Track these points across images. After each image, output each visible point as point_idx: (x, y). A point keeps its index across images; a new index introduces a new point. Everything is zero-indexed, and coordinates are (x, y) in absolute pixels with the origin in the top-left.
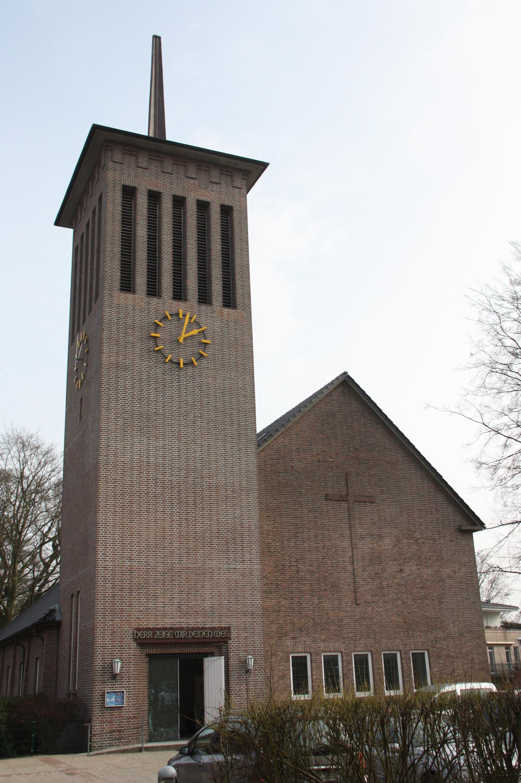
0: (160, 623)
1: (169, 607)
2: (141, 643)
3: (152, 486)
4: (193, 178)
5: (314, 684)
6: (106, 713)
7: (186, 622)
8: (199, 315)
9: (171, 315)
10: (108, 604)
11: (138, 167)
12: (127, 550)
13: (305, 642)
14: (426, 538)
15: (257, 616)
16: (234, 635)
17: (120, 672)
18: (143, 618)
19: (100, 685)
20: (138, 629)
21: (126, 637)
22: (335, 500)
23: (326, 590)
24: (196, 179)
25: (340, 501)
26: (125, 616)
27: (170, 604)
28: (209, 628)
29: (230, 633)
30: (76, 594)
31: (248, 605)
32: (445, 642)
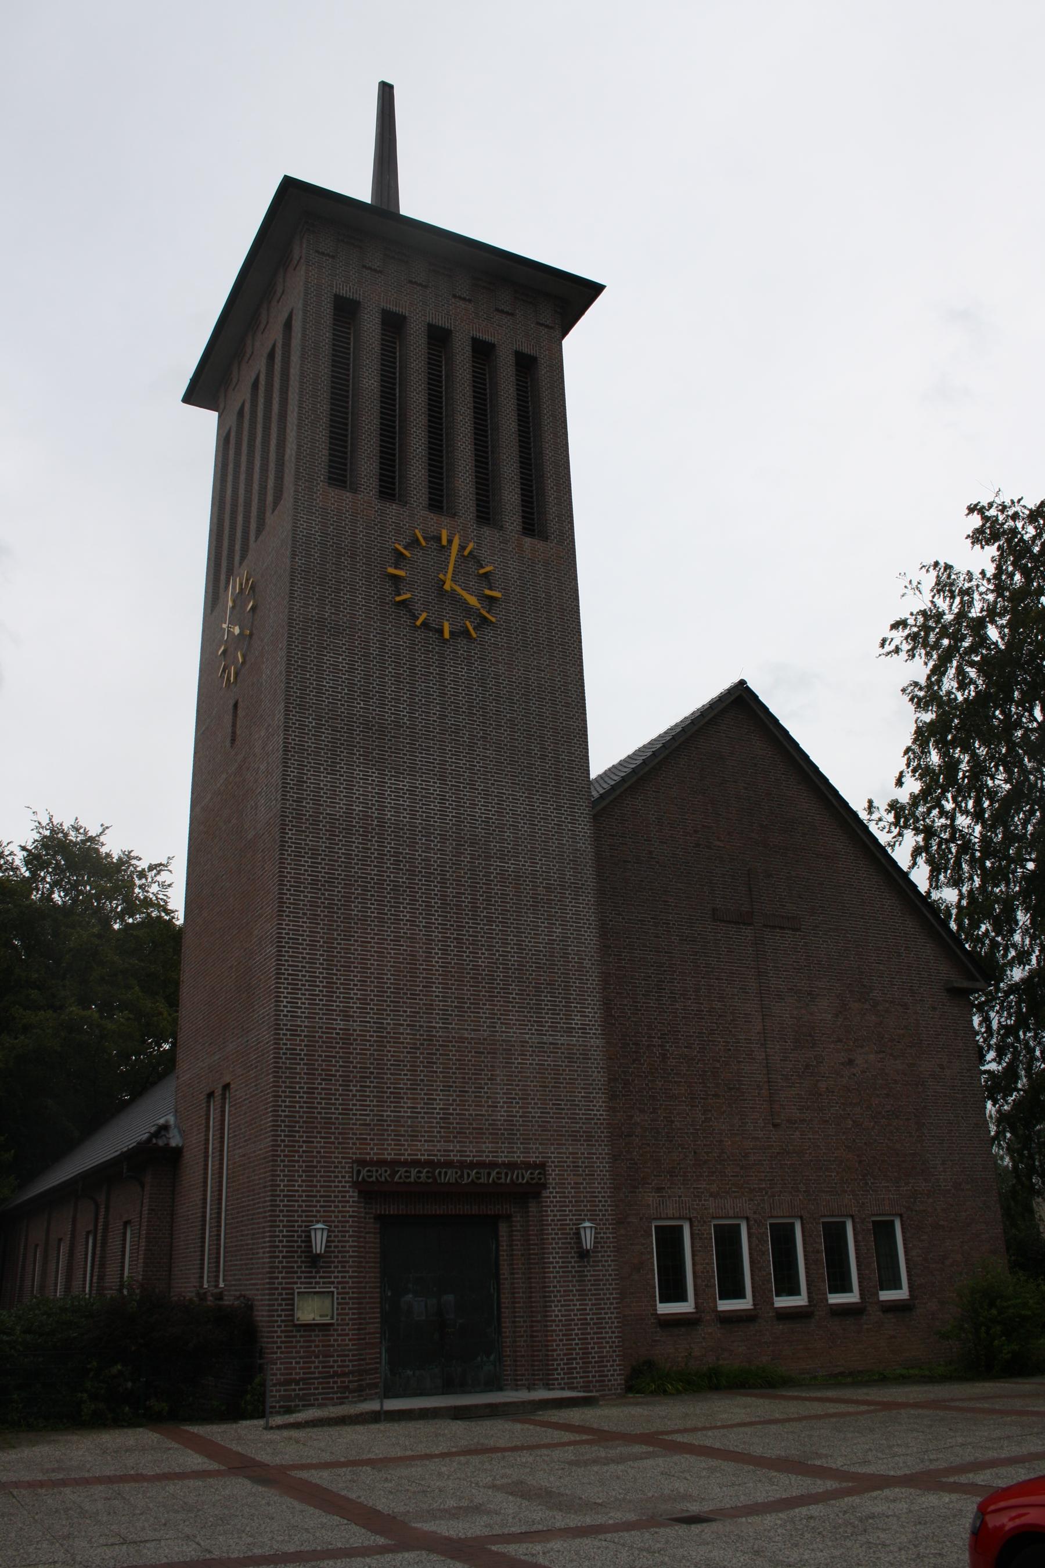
0: (406, 1150)
1: (423, 1118)
2: (368, 1192)
3: (388, 868)
4: (464, 299)
5: (699, 1281)
6: (296, 1336)
7: (458, 1151)
8: (479, 545)
9: (424, 538)
10: (301, 1107)
11: (364, 267)
12: (338, 997)
13: (680, 1197)
14: (891, 1002)
15: (597, 1141)
16: (554, 1179)
17: (325, 1251)
18: (372, 1139)
19: (283, 1278)
20: (362, 1163)
21: (337, 1177)
22: (730, 922)
23: (716, 1095)
24: (470, 301)
25: (738, 923)
26: (334, 1133)
27: (425, 1113)
28: (504, 1164)
29: (545, 1175)
30: (218, 1092)
31: (581, 1119)
32: (931, 1200)
